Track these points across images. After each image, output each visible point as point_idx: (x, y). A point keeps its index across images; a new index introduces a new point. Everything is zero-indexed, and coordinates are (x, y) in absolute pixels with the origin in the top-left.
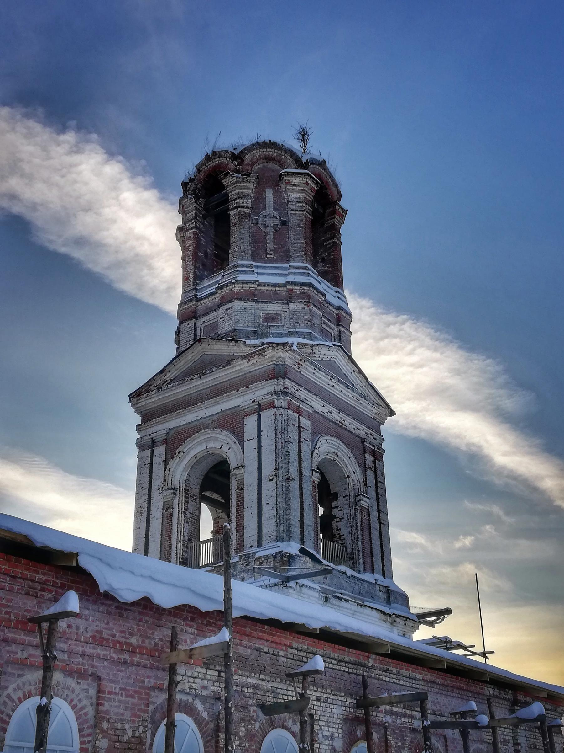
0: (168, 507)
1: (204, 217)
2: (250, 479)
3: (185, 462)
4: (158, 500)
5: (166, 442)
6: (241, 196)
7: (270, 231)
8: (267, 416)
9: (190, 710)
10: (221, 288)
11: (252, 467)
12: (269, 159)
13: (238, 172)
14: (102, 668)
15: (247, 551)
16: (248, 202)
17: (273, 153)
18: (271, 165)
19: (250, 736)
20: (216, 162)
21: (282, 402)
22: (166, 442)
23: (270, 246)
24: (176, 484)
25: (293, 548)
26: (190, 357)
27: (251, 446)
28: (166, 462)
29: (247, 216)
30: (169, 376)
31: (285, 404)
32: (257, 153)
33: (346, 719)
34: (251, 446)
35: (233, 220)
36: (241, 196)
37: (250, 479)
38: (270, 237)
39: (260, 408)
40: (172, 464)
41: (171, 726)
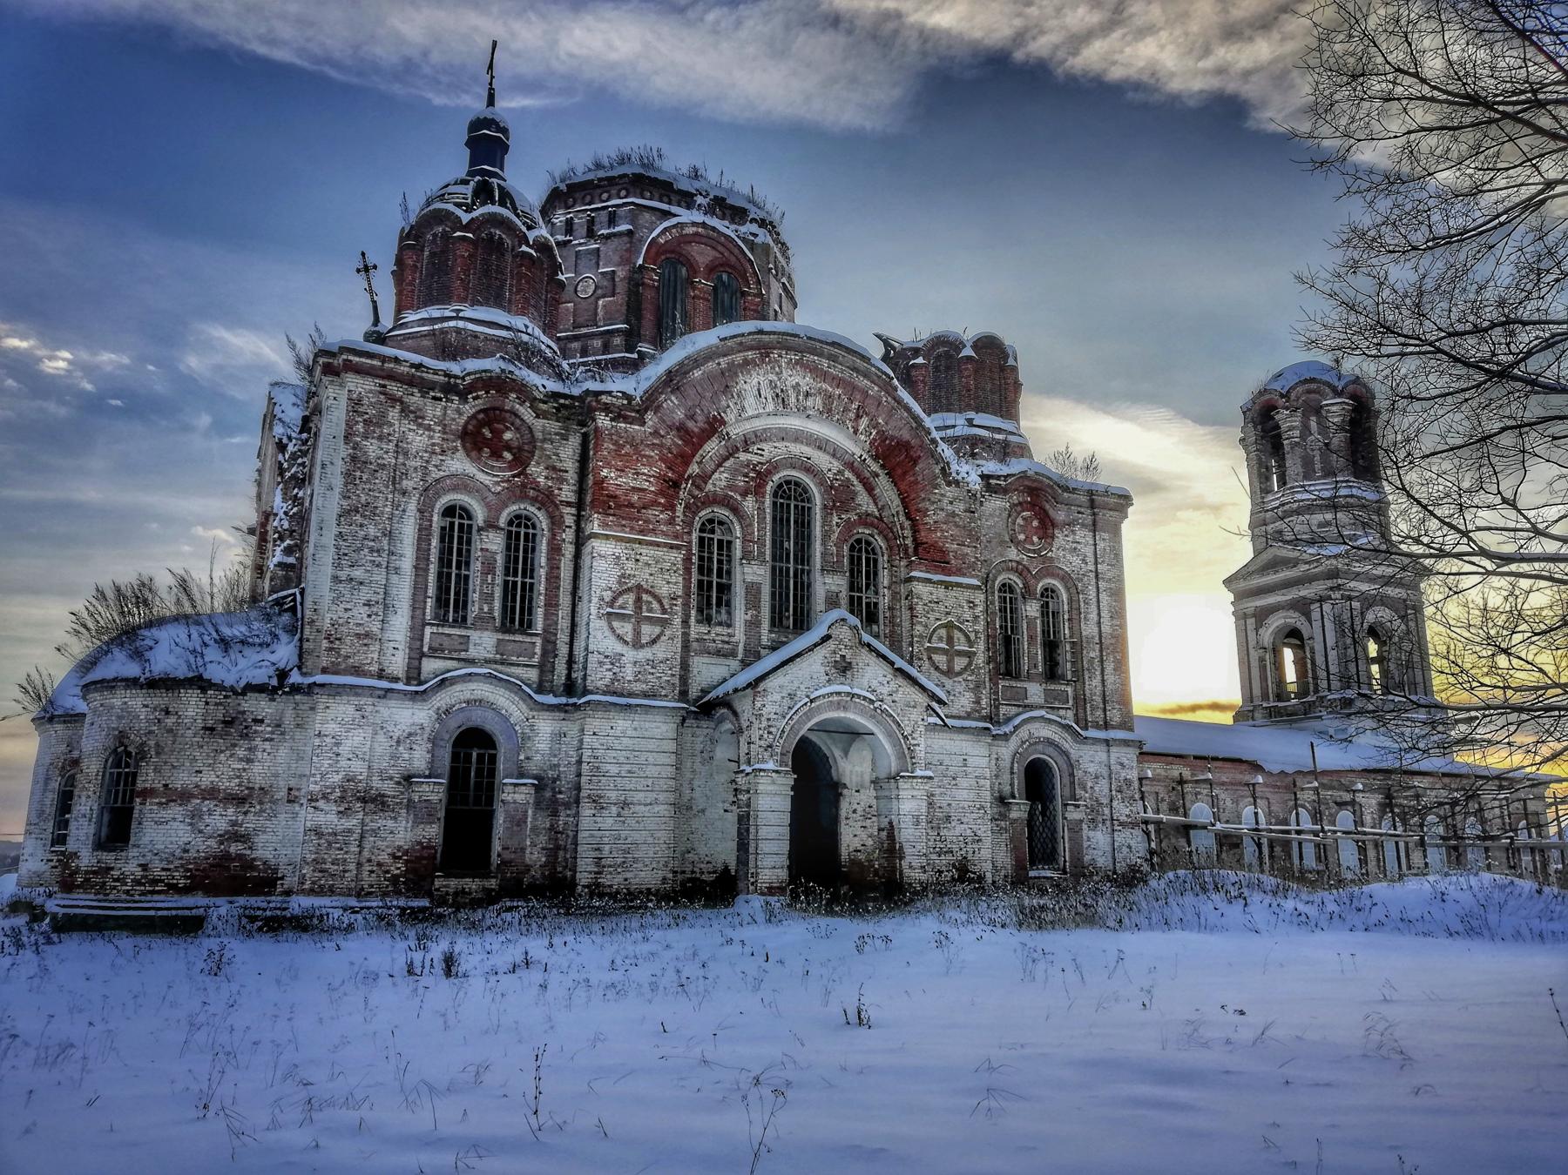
0: (1262, 660)
1: (1262, 438)
2: (1319, 647)
3: (1271, 630)
4: (1254, 655)
5: (1254, 615)
6: (1291, 429)
7: (1317, 453)
8: (1327, 607)
9: (1303, 807)
10: (1283, 505)
11: (1319, 638)
12: (1309, 392)
13: (1287, 408)
14: (1269, 795)
15: (1321, 694)
16: (1297, 433)
17: (1313, 386)
18: (1312, 396)
19: (1331, 815)
20: (1267, 397)
21: (1337, 595)
22: (1254, 615)
23: (1318, 466)
24: (1266, 645)
25: (1350, 694)
26: (1267, 556)
27: (1317, 625)
28: (1257, 630)
29: (1297, 444)
30: (1251, 569)
31: (1339, 596)
32: (1300, 389)
33: (1380, 804)
34: (1317, 625)
35: (1287, 448)
36: (1291, 429)
37: (1319, 647)
38: (1317, 458)
39: (1321, 600)
40: (1261, 631)
41: (1297, 814)
